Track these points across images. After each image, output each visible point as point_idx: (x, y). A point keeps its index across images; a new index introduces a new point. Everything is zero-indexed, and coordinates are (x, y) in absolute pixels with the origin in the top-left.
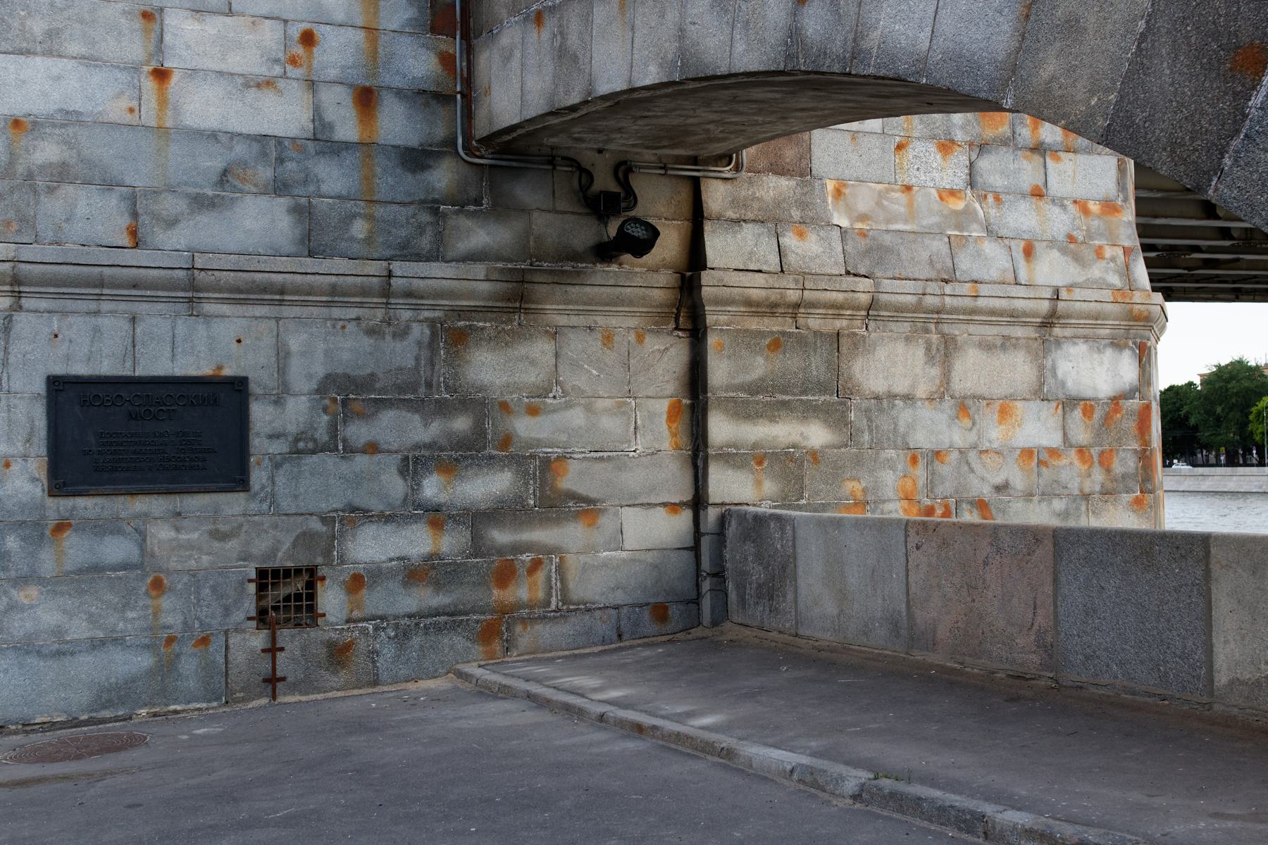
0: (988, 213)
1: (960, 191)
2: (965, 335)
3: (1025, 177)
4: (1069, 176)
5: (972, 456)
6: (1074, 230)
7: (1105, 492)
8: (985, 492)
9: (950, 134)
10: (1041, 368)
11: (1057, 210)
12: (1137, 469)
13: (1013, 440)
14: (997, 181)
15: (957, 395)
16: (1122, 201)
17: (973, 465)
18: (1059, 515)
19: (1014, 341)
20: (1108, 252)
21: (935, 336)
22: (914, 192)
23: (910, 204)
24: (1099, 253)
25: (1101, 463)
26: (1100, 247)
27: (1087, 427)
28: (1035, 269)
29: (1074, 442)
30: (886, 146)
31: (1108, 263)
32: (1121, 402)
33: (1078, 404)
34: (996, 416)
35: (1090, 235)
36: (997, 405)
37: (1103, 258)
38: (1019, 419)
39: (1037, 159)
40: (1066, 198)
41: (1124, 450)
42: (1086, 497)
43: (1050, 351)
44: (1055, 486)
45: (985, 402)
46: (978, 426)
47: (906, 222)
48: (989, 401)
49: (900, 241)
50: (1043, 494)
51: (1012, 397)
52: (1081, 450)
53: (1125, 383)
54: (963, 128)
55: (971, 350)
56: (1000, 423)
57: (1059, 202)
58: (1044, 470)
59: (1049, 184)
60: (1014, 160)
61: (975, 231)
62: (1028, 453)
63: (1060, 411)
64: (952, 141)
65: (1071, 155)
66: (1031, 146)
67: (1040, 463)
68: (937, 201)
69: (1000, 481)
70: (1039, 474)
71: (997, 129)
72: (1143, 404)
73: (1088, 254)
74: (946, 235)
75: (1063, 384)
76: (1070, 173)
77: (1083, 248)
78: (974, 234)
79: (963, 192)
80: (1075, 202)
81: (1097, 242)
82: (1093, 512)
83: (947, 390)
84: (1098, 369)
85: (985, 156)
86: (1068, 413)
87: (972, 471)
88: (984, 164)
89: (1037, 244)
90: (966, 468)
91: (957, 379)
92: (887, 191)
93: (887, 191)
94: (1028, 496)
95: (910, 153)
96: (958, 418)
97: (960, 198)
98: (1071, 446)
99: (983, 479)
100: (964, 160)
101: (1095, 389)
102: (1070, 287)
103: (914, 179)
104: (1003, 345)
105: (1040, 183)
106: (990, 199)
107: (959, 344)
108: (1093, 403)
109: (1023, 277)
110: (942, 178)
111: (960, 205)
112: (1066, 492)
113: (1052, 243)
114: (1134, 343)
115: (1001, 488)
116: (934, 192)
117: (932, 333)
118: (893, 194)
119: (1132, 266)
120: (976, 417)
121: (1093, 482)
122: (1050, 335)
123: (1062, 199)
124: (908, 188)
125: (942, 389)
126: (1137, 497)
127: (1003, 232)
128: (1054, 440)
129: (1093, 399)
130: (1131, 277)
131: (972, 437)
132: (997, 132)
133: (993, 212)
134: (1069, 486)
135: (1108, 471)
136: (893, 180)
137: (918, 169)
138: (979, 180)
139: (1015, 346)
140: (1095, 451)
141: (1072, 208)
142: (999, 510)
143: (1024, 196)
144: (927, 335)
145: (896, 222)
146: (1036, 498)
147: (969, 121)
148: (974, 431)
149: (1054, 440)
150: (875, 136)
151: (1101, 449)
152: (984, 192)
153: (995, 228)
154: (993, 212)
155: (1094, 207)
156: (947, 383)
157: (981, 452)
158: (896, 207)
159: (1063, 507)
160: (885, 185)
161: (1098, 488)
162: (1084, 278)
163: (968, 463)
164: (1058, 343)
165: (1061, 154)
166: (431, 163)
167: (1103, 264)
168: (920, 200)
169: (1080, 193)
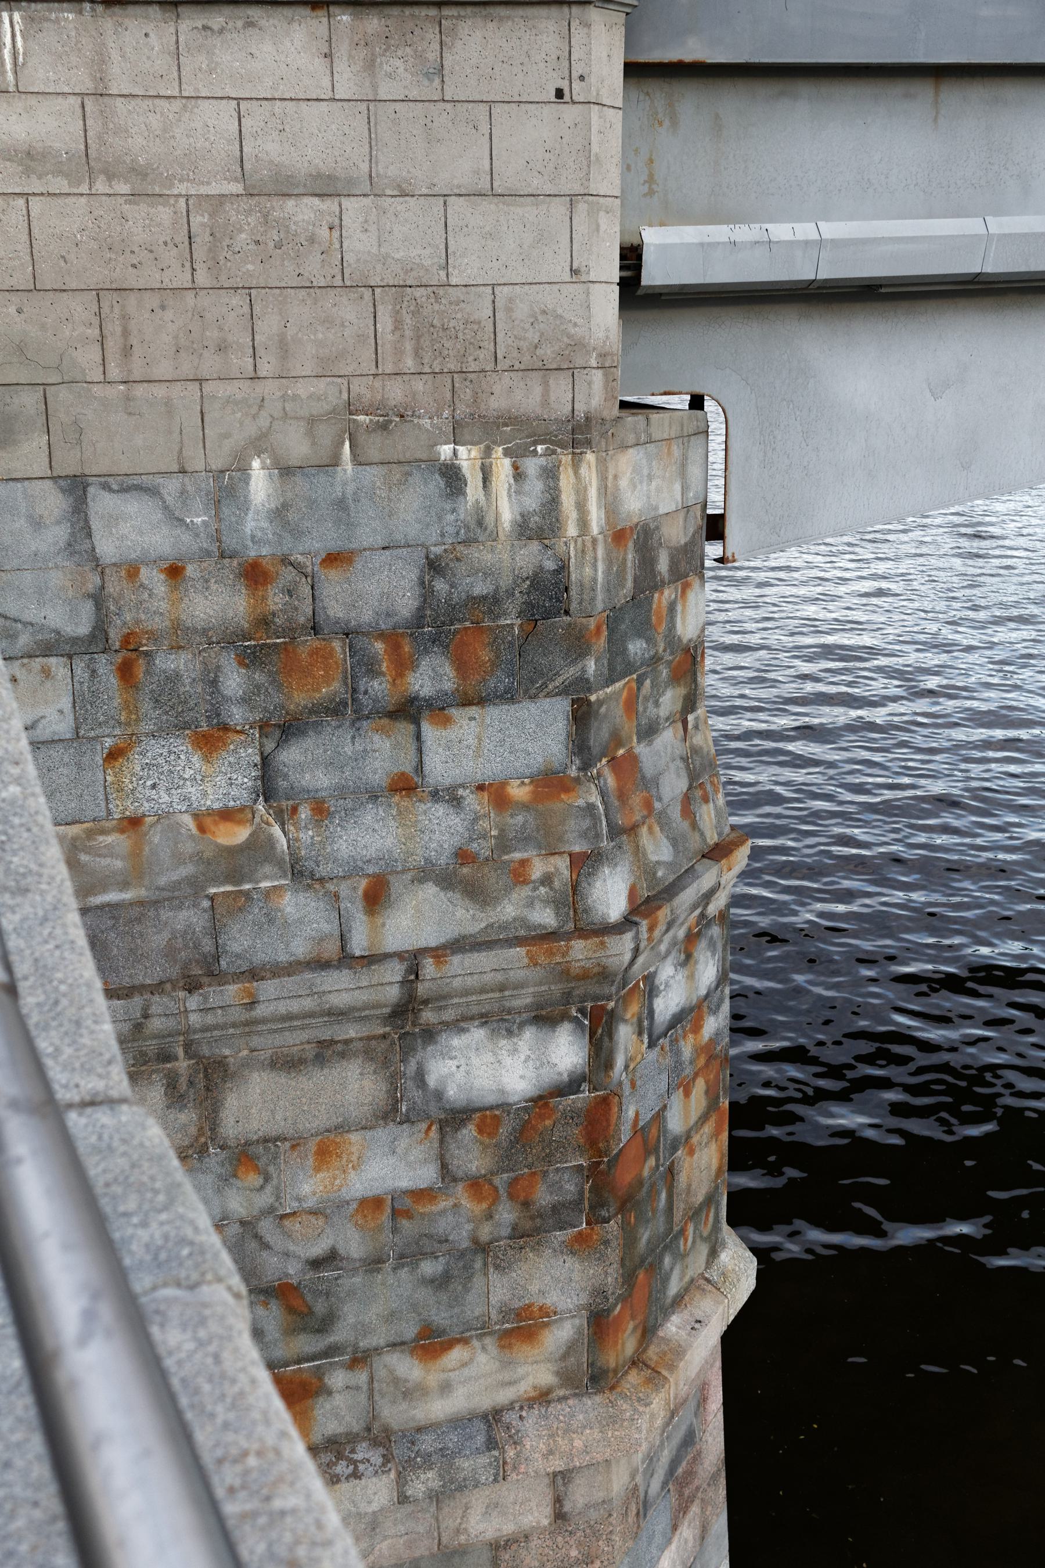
0: (297, 840)
1: (242, 809)
2: (245, 1052)
3: (377, 764)
4: (468, 747)
5: (266, 1227)
6: (471, 840)
7: (518, 1234)
8: (291, 1272)
9: (218, 715)
10: (394, 1080)
11: (440, 810)
12: (581, 1193)
13: (344, 1190)
14: (320, 780)
15: (232, 1143)
16: (579, 769)
17: (268, 1238)
18: (432, 1281)
19: (340, 1047)
20: (538, 869)
21: (185, 1064)
22: (145, 828)
23: (135, 854)
24: (519, 875)
25: (511, 1197)
26: (524, 863)
27: (486, 1147)
28: (384, 925)
29: (460, 1174)
30: (85, 759)
31: (535, 889)
32: (553, 1101)
33: (469, 1119)
34: (310, 1161)
35: (504, 844)
36: (312, 1146)
37: (526, 882)
38: (354, 1158)
39: (405, 728)
40: (463, 786)
41: (557, 1170)
42: (481, 1248)
43: (414, 1049)
44: (425, 1241)
45: (288, 1144)
46: (275, 1182)
47: (125, 885)
48: (296, 1143)
49: (110, 923)
50: (402, 1256)
51: (342, 1128)
52: (476, 1185)
53: (560, 1074)
54: (245, 701)
55: (255, 1075)
56: (317, 1169)
57: (450, 796)
58: (405, 1223)
59: (427, 769)
60: (353, 737)
61: (266, 877)
62: (372, 1204)
63: (434, 1133)
64: (225, 728)
65: (473, 711)
66: (390, 708)
67: (395, 1213)
68: (192, 837)
69: (321, 1252)
70: (395, 1230)
71: (318, 690)
72: (595, 1097)
73: (493, 880)
74: (207, 896)
75: (439, 1095)
76: (471, 741)
77: (486, 870)
78: (265, 884)
79: (248, 811)
80: (481, 788)
81: (517, 856)
82: (497, 1267)
83: (212, 1140)
84: (508, 1061)
85: (293, 741)
86: (448, 1139)
87: (266, 1246)
88: (291, 755)
89: (392, 879)
90: (254, 1245)
91: (231, 1120)
92: (90, 834)
93: (90, 834)
94: (374, 1263)
95: (136, 762)
96: (235, 1176)
97: (240, 822)
98: (455, 1180)
99: (287, 1254)
100: (250, 754)
101: (502, 1092)
102: (440, 953)
103: (146, 804)
104: (318, 1056)
105: (408, 768)
106: (304, 813)
107: (232, 1068)
108: (497, 1113)
109: (358, 945)
110: (205, 794)
111: (241, 834)
112: (445, 1247)
113: (425, 873)
114: (582, 1011)
115: (330, 1259)
116: (188, 820)
117: (176, 1059)
118: (101, 838)
119: (584, 884)
120: (271, 1169)
121: (499, 1225)
122: (414, 1024)
123: (452, 789)
124: (134, 822)
125: (203, 1140)
126: (580, 1233)
127: (323, 871)
128: (426, 1175)
129: (498, 1106)
130: (580, 906)
131: (265, 1199)
132: (317, 695)
133: (306, 836)
134: (451, 1238)
135: (526, 1204)
136: (103, 814)
137: (154, 786)
138: (283, 784)
139: (343, 1055)
140: (501, 1181)
141: (472, 801)
142: (317, 1293)
143: (374, 797)
144: (168, 1066)
145: (104, 889)
146: (387, 1266)
147: (258, 687)
148: (269, 1189)
149: (426, 1175)
150: (60, 747)
151: (512, 1175)
152: (291, 802)
153: (310, 864)
154: (306, 836)
155: (518, 792)
156: (212, 1130)
157: (283, 1217)
158: (105, 862)
159: (440, 1268)
160: (86, 825)
161: (505, 1232)
162: (483, 925)
163: (257, 1237)
164: (429, 1035)
165: (454, 712)
166: (263, 23)
167: (526, 891)
168: (156, 840)
169: (488, 770)
